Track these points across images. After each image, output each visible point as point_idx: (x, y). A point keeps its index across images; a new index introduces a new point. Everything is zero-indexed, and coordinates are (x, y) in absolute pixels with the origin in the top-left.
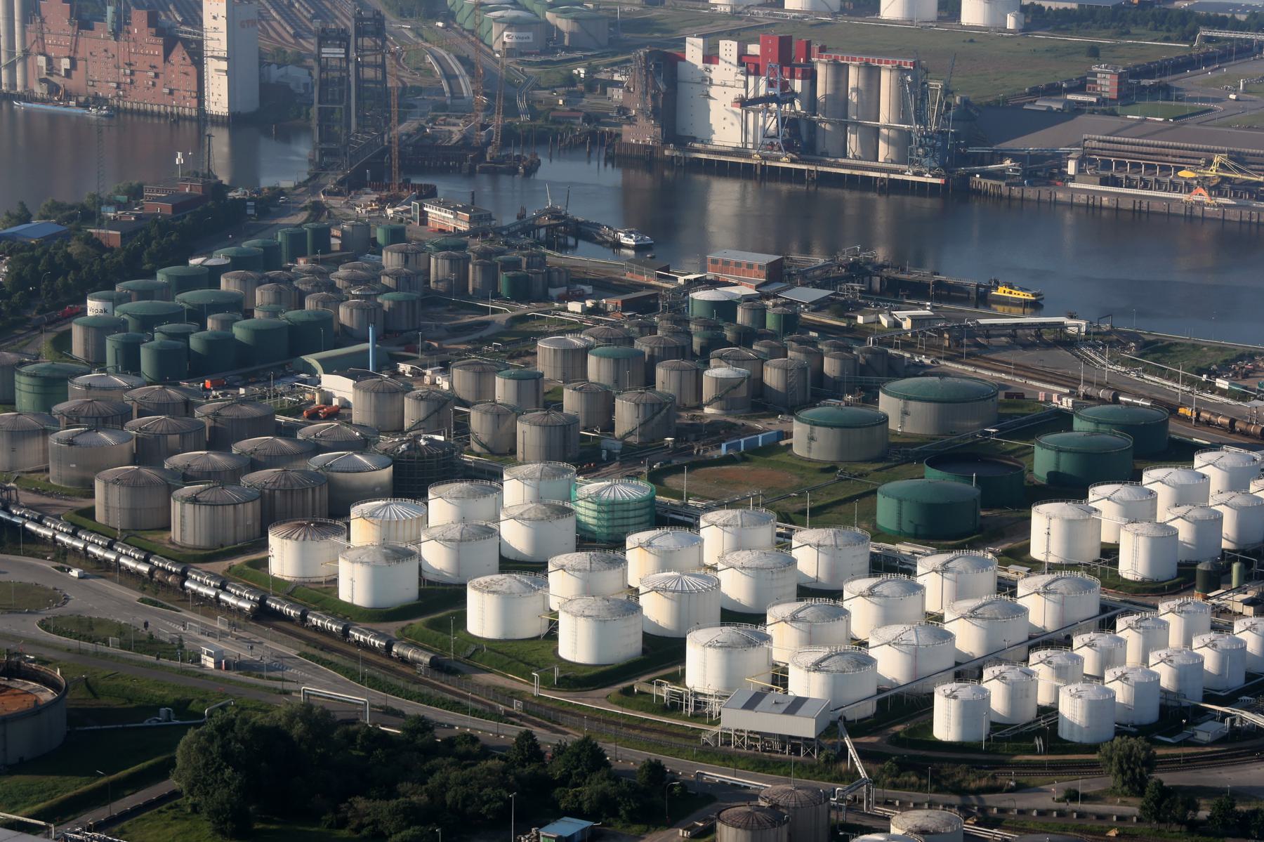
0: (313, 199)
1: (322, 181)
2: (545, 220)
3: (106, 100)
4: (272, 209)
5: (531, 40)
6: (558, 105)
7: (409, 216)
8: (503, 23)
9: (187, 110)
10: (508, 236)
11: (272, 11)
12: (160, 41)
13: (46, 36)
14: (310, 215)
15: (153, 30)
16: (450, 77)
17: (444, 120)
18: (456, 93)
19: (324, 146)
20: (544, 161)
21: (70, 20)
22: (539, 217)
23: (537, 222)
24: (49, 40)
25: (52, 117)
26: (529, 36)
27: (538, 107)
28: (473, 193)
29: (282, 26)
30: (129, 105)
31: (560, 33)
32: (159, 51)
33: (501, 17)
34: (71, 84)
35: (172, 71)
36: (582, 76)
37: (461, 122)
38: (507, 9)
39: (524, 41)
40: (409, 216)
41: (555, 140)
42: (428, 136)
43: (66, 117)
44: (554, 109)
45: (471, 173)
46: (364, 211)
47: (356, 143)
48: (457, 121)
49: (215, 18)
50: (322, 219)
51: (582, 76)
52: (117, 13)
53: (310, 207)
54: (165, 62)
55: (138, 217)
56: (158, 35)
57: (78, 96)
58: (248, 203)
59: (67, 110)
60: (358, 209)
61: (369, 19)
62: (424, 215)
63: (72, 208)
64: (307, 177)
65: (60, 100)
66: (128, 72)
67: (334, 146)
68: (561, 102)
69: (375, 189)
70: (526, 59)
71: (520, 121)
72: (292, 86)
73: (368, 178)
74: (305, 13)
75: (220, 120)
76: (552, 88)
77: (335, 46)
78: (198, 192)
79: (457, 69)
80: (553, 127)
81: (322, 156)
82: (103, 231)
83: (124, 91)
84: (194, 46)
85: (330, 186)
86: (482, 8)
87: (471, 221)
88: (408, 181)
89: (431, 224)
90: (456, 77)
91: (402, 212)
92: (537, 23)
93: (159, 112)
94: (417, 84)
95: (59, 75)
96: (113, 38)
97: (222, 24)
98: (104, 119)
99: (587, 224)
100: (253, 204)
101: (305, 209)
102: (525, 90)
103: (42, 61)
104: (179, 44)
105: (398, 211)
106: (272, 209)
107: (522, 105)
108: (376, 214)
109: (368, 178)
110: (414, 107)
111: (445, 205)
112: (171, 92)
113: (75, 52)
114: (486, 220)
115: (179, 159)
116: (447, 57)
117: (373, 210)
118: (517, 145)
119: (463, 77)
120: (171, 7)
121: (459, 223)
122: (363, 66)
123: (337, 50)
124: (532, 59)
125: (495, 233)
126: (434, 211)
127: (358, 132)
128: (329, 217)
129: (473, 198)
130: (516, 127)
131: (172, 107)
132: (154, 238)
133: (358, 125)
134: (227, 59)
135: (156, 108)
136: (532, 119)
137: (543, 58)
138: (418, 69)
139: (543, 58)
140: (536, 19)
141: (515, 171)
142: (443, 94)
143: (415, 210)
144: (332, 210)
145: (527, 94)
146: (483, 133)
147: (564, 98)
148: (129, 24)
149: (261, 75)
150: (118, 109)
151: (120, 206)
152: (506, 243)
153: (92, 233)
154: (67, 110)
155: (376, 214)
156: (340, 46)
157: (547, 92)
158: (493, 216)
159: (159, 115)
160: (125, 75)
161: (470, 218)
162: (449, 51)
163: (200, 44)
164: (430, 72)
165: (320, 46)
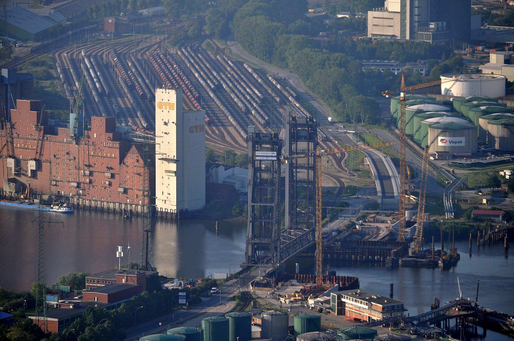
0: (242, 290)
1: (253, 273)
2: (455, 311)
3: (67, 198)
4: (202, 299)
5: (463, 144)
6: (481, 204)
7: (328, 306)
8: (437, 128)
9: (139, 207)
10: (418, 325)
11: (230, 118)
12: (117, 144)
13: (15, 140)
14: (238, 305)
15: (111, 135)
16: (383, 177)
17: (373, 217)
18: (386, 193)
19: (256, 241)
20: (464, 256)
21: (37, 126)
22: (448, 308)
23: (447, 313)
24: (18, 143)
25: (19, 214)
26: (462, 141)
27: (463, 206)
28: (392, 285)
29: (237, 131)
30: (87, 203)
31: (492, 138)
32: (116, 154)
33: (436, 123)
34: (36, 184)
35: (127, 172)
36: (507, 177)
37: (389, 219)
38: (442, 116)
39: (457, 145)
40: (328, 306)
41: (475, 237)
42: (358, 233)
43: (31, 213)
44: (476, 208)
45: (394, 267)
46: (287, 301)
47: (290, 239)
48: (385, 218)
49: (166, 124)
50: (247, 309)
51: (507, 177)
52: (78, 120)
53: (238, 297)
54: (120, 163)
55: (77, 306)
56: (114, 139)
57: (42, 194)
58: (180, 294)
59: (31, 207)
60: (282, 300)
61: (302, 125)
62: (342, 305)
63: (18, 297)
64: (241, 269)
65: (26, 198)
66: (87, 172)
67: (266, 241)
68: (484, 201)
69: (301, 281)
70: (458, 161)
71: (444, 219)
72: (237, 186)
73: (297, 271)
74: (260, 119)
75: (169, 216)
76: (478, 189)
77: (267, 149)
78: (134, 283)
79: (391, 169)
80: (475, 224)
81: (254, 250)
82: (42, 318)
83: (84, 190)
84: (147, 149)
85: (259, 278)
86: (420, 115)
87: (384, 311)
88: (334, 273)
89: (348, 314)
90: (389, 178)
91: (322, 303)
92: (469, 128)
93: (115, 209)
94: (353, 184)
95: (26, 175)
96: (74, 142)
97: (173, 129)
98: (62, 215)
99: (494, 314)
100: (185, 294)
101: (233, 299)
102: (451, 191)
103: (11, 162)
104: (134, 148)
105: (318, 302)
106: (202, 299)
107: (448, 204)
108: (299, 304)
109: (297, 271)
110: (347, 205)
111: (361, 297)
112: (126, 191)
113: (41, 154)
114: (398, 311)
115: (119, 252)
116: (383, 159)
117: (296, 301)
118: (437, 240)
119: (394, 177)
120: (139, 114)
121: (373, 313)
122: (297, 168)
123: (270, 153)
124: (463, 161)
125: (406, 323)
126: (351, 302)
127: (291, 228)
128: (255, 306)
129: (392, 290)
130: (440, 224)
131: (126, 204)
132: (89, 325)
133: (291, 220)
134: (176, 161)
135: (111, 205)
136: (456, 217)
137: (473, 161)
138: (357, 170)
139: (473, 161)
140: (469, 125)
141: (435, 265)
142: (375, 193)
143: (334, 301)
144: (259, 300)
145: (453, 193)
146: (408, 230)
147: (489, 197)
148: (90, 129)
149: (208, 177)
150: (78, 207)
151: (63, 295)
152: (416, 332)
153: (32, 320)
154: (31, 207)
155: (299, 304)
156: (272, 150)
157: (473, 192)
158: (405, 307)
159: (114, 212)
160: (85, 175)
161: (383, 308)
162: (386, 154)
163: (153, 146)
164: (368, 172)
165: (254, 150)
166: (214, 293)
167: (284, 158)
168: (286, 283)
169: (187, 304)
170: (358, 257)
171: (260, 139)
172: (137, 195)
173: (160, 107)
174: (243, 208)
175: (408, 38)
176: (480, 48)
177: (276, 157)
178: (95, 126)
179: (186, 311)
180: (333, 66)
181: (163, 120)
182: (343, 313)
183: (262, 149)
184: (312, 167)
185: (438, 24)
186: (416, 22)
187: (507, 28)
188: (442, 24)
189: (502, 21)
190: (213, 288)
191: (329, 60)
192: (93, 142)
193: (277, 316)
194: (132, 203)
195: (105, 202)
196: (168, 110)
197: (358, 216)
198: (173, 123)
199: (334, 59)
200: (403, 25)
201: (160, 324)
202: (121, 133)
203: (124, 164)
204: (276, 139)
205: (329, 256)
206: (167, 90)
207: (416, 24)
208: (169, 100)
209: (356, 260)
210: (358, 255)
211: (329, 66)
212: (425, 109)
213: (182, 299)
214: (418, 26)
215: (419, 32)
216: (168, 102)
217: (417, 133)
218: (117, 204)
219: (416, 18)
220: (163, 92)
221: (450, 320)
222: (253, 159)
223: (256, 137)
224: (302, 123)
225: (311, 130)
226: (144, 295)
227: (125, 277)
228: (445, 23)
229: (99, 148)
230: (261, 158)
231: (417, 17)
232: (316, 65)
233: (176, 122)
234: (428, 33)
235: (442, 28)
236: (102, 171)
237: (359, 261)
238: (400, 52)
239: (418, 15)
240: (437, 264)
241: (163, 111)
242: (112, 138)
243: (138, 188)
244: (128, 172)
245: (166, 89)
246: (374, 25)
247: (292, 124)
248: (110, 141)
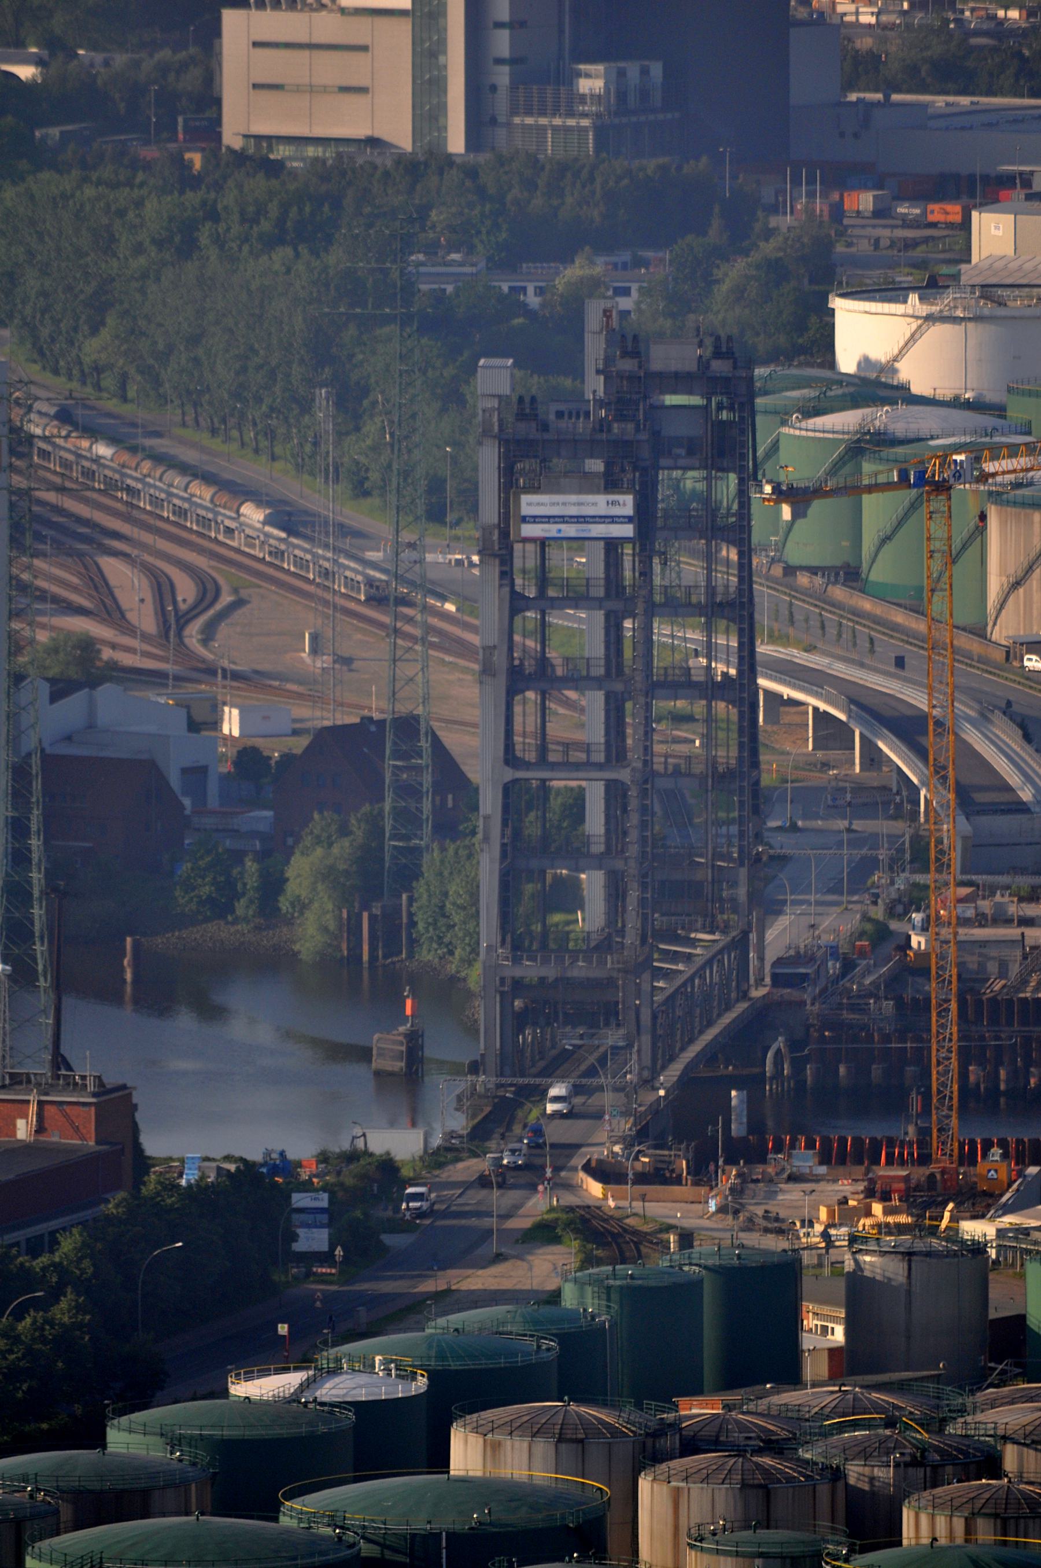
4: (387, 1239)
77: (587, 484)
123: (599, 503)
156: (611, 484)
166: (420, 1214)
167: (776, 489)
168: (760, 1168)
169: (339, 1251)
170: (1003, 1074)
171: (545, 427)
174: (235, 872)
175: (456, 143)
176: (866, 200)
177: (629, 519)
179: (334, 1288)
180: (246, 248)
184: (731, 604)
185: (621, 74)
186: (499, 61)
187: (965, 101)
188: (645, 72)
189: (924, 69)
190: (410, 1190)
191: (213, 215)
193: (934, 1261)
197: (894, 895)
199: (242, 213)
200: (430, 81)
201: (283, 1329)
204: (630, 427)
205: (842, 1070)
207: (502, 76)
209: (994, 1092)
210: (999, 1063)
211: (222, 247)
212: (899, 429)
213: (308, 1226)
214: (514, 87)
215: (517, 120)
217: (888, 548)
219: (502, 43)
222: (505, 534)
223: (521, 416)
224: (674, 366)
225: (720, 407)
226: (158, 1194)
227: (33, 1109)
228: (657, 70)
230: (550, 530)
231: (504, 35)
232: (139, 249)
234: (571, 122)
235: (644, 94)
237: (1005, 1093)
238: (477, 211)
239: (511, 25)
246: (255, 86)
247: (620, 376)
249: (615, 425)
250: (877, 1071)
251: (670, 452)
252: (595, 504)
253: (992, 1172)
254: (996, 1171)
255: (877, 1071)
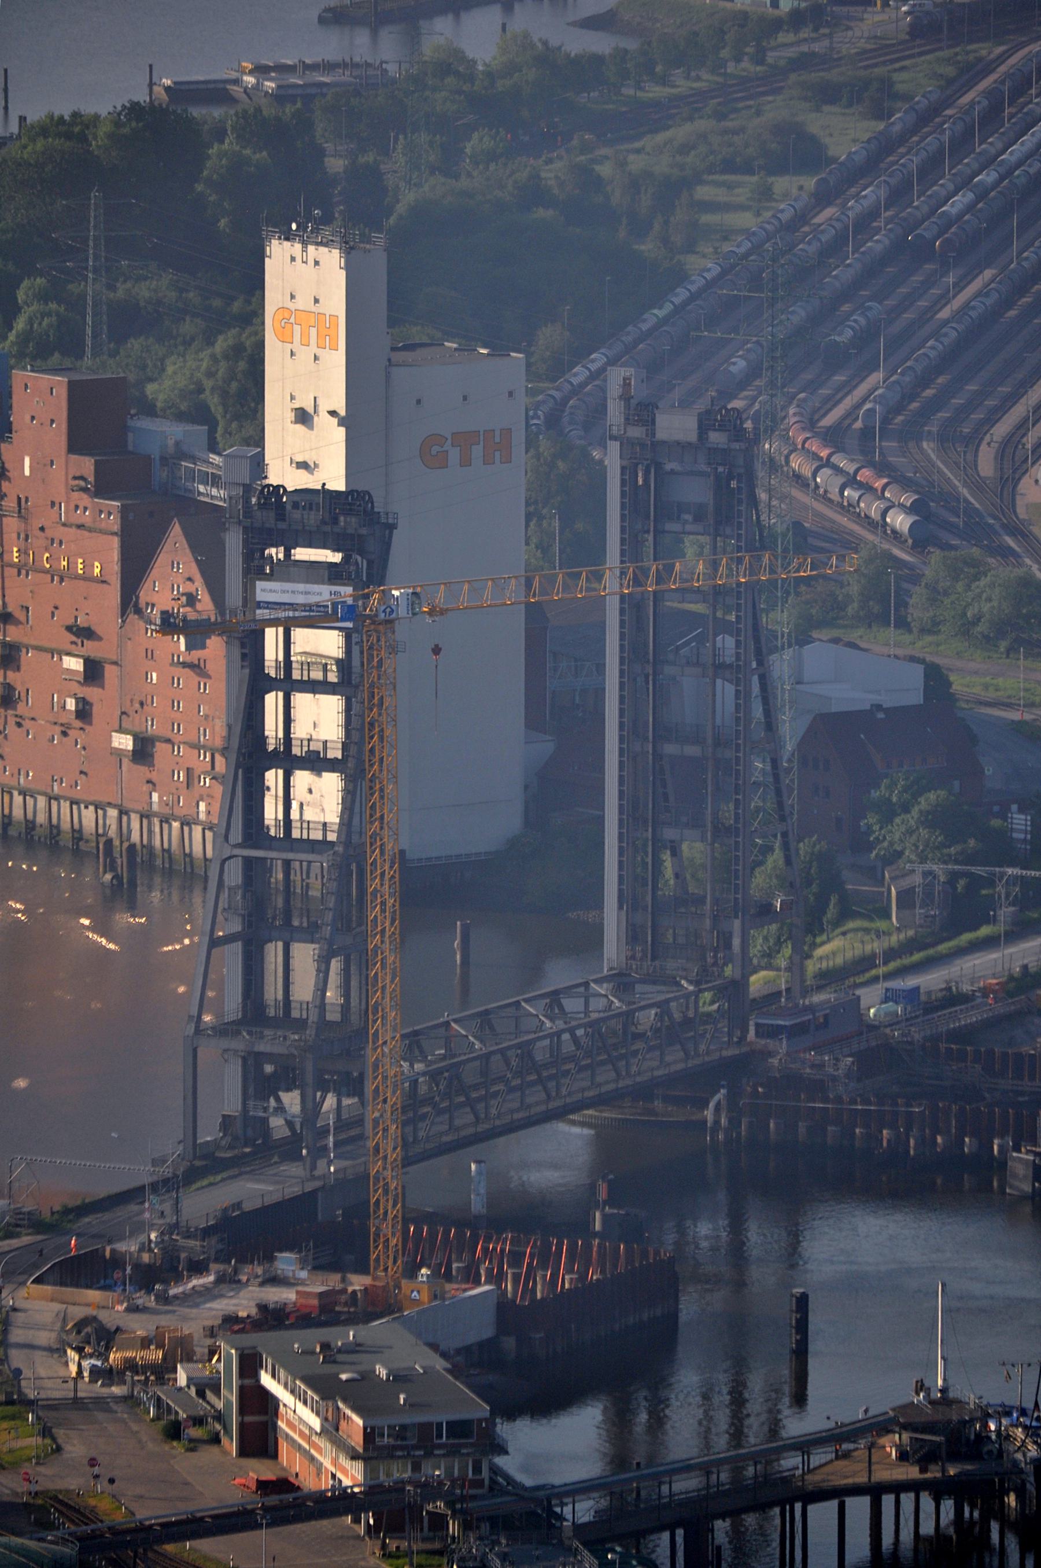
15: (86, 465)
49: (303, 417)
54: (124, 613)
56: (102, 488)
172: (189, 771)
173: (285, 338)
178: (28, 418)
181: (292, 398)
182: (271, 1449)
183: (289, 569)
192: (19, 499)
194: (167, 811)
195: (66, 799)
196: (313, 349)
198: (333, 413)
202: (148, 460)
203: (138, 611)
206: (311, 248)
208: (316, 301)
210: (908, 1129)
216: (310, 306)
218: (113, 813)
220: (293, 259)
221: (810, 1508)
224: (679, 436)
229: (42, 529)
233: (343, 412)
236: (53, 645)
240: (589, 1222)
241: (292, 354)
242: (91, 479)
243: (192, 738)
244: (156, 653)
245: (305, 244)
248: (85, 496)
249: (342, 518)
250: (802, 1127)
251: (679, 518)
252: (320, 594)
253: (415, 1293)
254: (418, 1292)
255: (802, 1127)
